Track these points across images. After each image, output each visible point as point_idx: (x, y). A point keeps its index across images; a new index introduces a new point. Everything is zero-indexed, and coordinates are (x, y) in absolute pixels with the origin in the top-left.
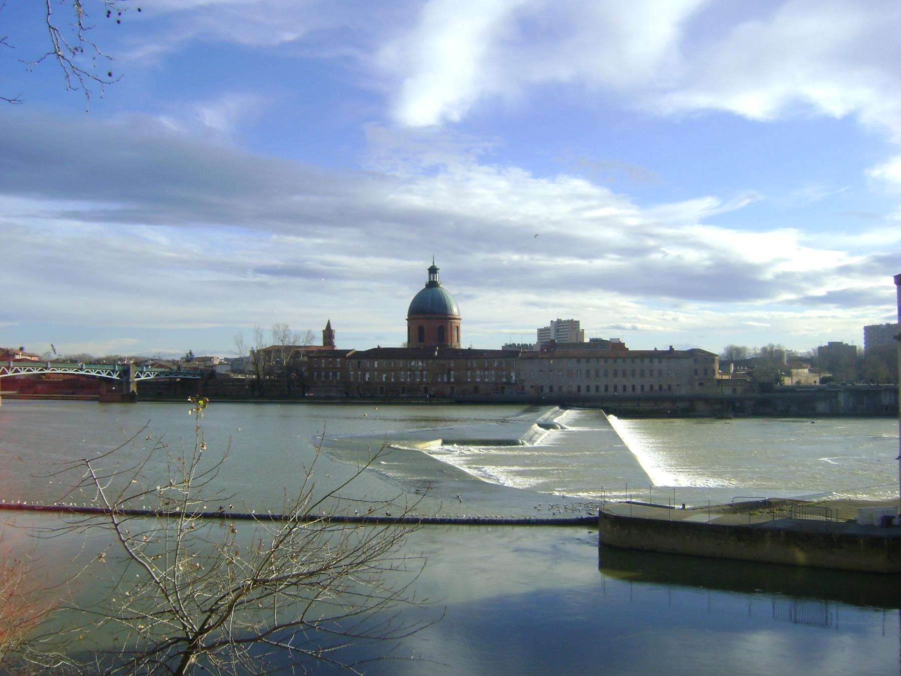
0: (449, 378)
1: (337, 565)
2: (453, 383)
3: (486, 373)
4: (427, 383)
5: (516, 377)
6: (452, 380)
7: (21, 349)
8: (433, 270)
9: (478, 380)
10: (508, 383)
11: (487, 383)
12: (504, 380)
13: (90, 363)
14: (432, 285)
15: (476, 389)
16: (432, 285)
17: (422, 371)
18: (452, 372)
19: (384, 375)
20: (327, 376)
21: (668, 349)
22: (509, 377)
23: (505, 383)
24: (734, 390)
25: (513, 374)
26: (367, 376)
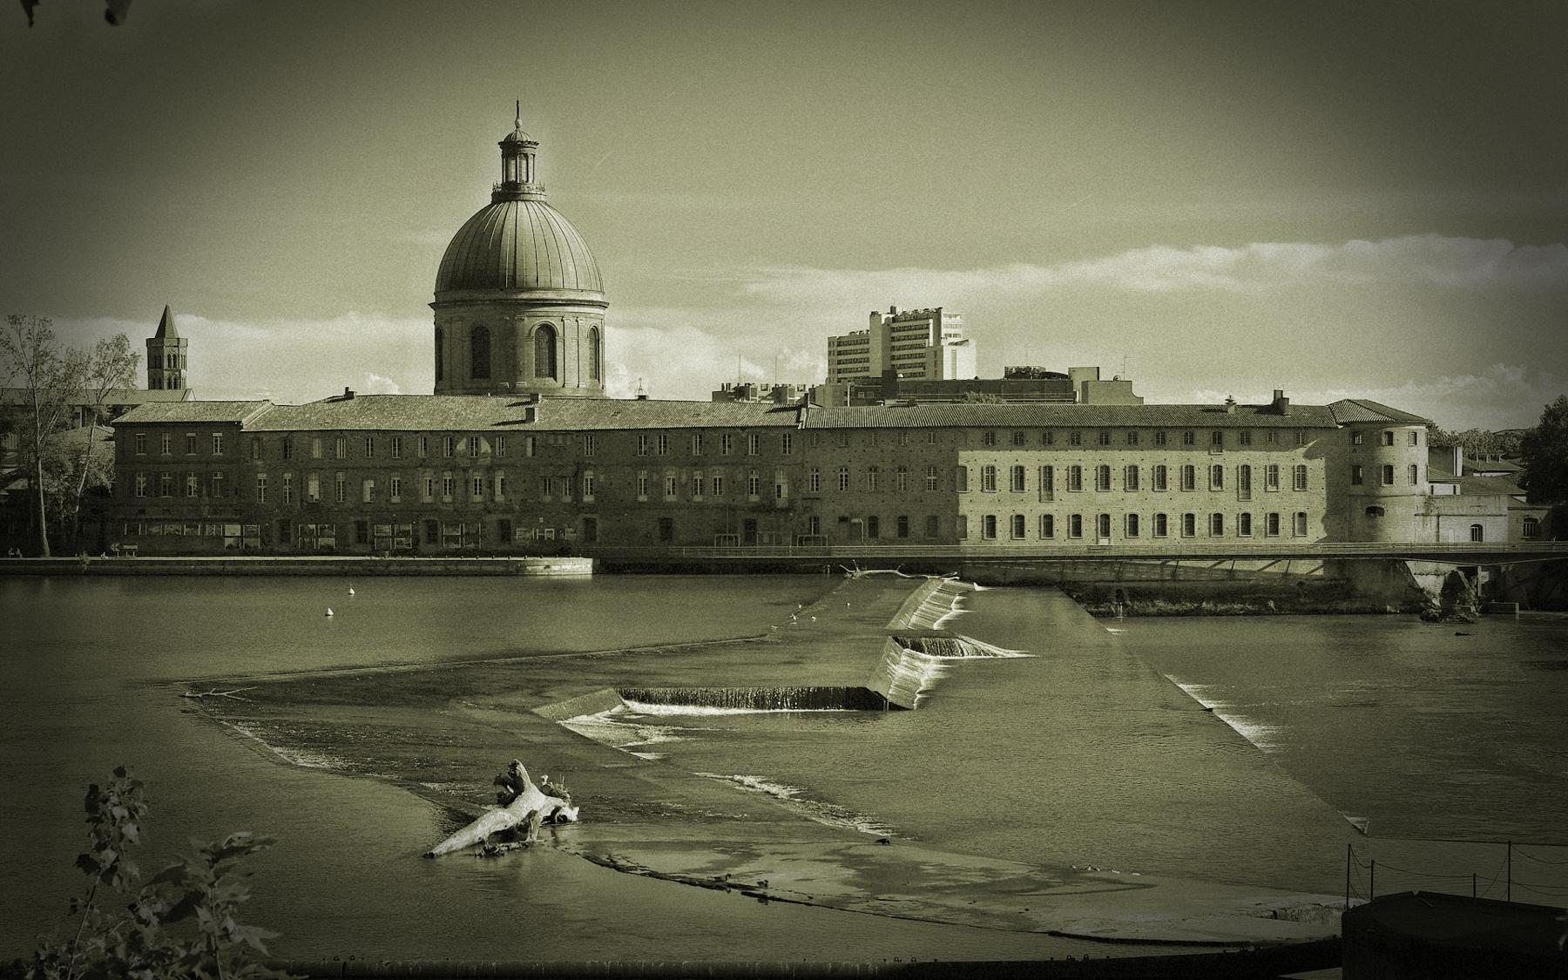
0: (577, 493)
1: (630, 772)
2: (590, 508)
3: (698, 476)
4: (509, 510)
5: (795, 484)
6: (588, 499)
7: (1230, 401)
8: (31, 23)
9: (671, 498)
10: (767, 508)
11: (701, 507)
12: (754, 498)
13: (334, 741)
14: (509, 192)
15: (667, 527)
16: (30, 15)
17: (491, 469)
18: (589, 474)
19: (369, 484)
20: (771, 537)
21: (432, 312)
22: (767, 487)
23: (756, 508)
24: (1477, 532)
25: (781, 480)
26: (314, 488)
